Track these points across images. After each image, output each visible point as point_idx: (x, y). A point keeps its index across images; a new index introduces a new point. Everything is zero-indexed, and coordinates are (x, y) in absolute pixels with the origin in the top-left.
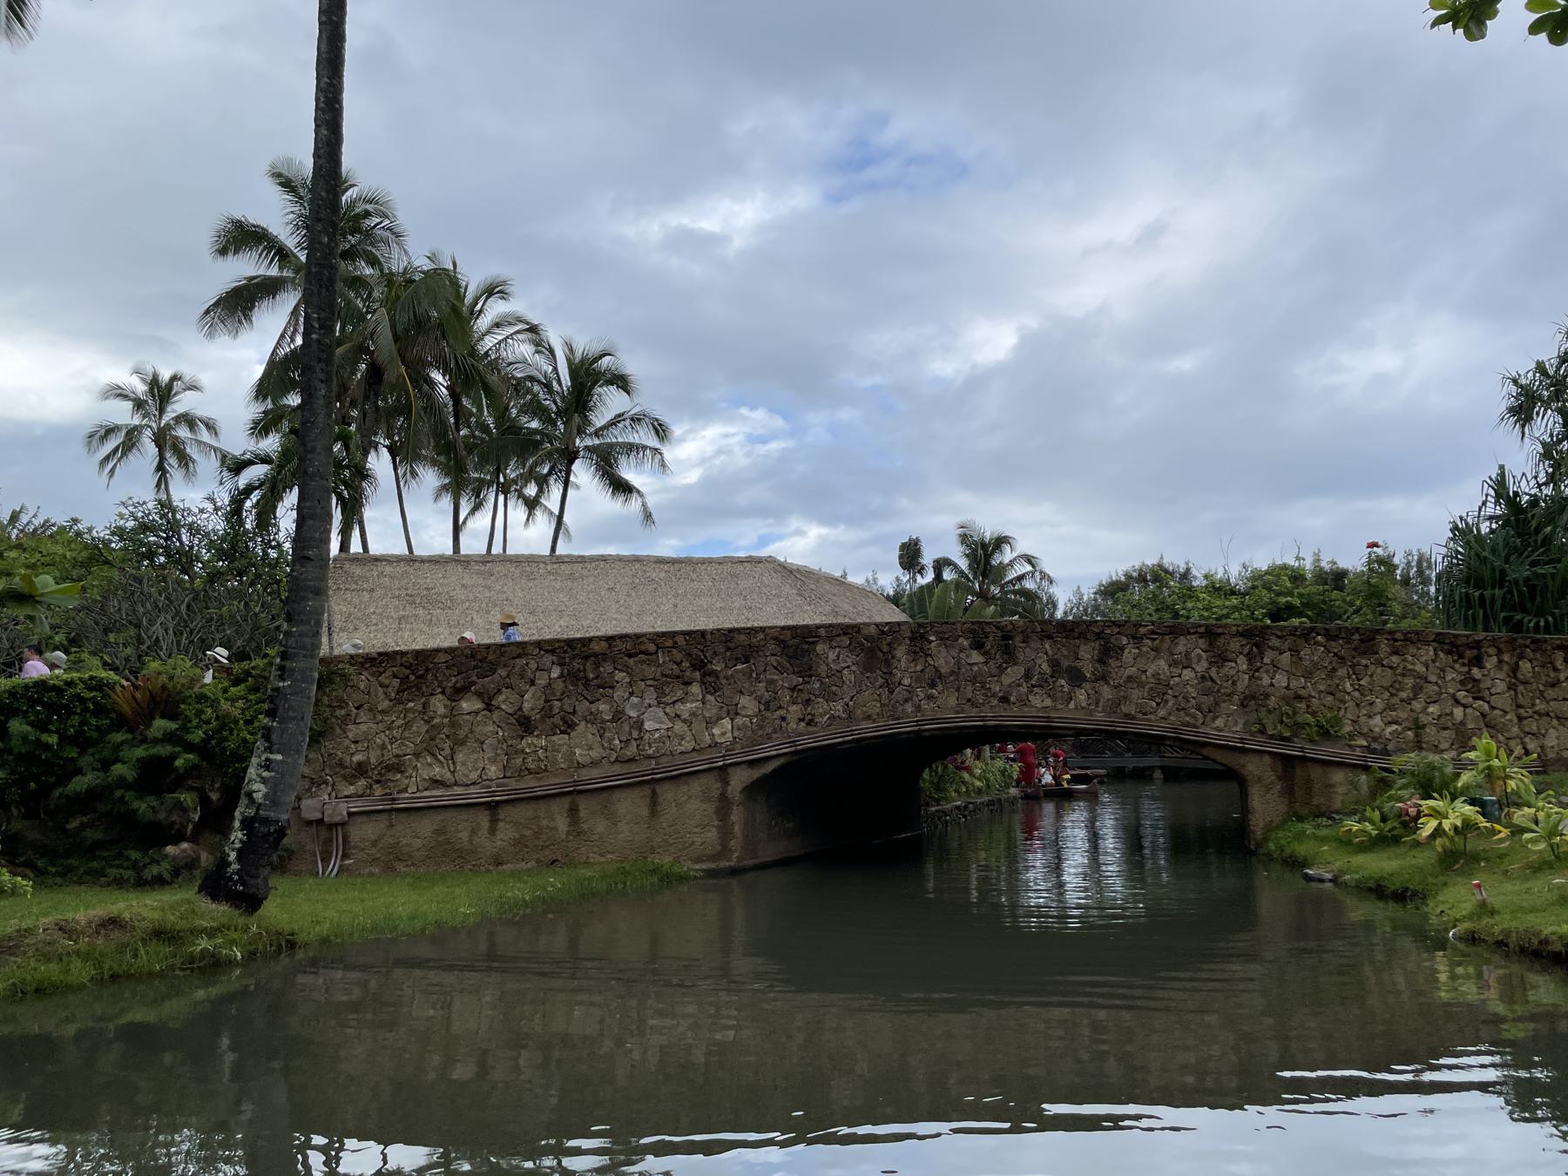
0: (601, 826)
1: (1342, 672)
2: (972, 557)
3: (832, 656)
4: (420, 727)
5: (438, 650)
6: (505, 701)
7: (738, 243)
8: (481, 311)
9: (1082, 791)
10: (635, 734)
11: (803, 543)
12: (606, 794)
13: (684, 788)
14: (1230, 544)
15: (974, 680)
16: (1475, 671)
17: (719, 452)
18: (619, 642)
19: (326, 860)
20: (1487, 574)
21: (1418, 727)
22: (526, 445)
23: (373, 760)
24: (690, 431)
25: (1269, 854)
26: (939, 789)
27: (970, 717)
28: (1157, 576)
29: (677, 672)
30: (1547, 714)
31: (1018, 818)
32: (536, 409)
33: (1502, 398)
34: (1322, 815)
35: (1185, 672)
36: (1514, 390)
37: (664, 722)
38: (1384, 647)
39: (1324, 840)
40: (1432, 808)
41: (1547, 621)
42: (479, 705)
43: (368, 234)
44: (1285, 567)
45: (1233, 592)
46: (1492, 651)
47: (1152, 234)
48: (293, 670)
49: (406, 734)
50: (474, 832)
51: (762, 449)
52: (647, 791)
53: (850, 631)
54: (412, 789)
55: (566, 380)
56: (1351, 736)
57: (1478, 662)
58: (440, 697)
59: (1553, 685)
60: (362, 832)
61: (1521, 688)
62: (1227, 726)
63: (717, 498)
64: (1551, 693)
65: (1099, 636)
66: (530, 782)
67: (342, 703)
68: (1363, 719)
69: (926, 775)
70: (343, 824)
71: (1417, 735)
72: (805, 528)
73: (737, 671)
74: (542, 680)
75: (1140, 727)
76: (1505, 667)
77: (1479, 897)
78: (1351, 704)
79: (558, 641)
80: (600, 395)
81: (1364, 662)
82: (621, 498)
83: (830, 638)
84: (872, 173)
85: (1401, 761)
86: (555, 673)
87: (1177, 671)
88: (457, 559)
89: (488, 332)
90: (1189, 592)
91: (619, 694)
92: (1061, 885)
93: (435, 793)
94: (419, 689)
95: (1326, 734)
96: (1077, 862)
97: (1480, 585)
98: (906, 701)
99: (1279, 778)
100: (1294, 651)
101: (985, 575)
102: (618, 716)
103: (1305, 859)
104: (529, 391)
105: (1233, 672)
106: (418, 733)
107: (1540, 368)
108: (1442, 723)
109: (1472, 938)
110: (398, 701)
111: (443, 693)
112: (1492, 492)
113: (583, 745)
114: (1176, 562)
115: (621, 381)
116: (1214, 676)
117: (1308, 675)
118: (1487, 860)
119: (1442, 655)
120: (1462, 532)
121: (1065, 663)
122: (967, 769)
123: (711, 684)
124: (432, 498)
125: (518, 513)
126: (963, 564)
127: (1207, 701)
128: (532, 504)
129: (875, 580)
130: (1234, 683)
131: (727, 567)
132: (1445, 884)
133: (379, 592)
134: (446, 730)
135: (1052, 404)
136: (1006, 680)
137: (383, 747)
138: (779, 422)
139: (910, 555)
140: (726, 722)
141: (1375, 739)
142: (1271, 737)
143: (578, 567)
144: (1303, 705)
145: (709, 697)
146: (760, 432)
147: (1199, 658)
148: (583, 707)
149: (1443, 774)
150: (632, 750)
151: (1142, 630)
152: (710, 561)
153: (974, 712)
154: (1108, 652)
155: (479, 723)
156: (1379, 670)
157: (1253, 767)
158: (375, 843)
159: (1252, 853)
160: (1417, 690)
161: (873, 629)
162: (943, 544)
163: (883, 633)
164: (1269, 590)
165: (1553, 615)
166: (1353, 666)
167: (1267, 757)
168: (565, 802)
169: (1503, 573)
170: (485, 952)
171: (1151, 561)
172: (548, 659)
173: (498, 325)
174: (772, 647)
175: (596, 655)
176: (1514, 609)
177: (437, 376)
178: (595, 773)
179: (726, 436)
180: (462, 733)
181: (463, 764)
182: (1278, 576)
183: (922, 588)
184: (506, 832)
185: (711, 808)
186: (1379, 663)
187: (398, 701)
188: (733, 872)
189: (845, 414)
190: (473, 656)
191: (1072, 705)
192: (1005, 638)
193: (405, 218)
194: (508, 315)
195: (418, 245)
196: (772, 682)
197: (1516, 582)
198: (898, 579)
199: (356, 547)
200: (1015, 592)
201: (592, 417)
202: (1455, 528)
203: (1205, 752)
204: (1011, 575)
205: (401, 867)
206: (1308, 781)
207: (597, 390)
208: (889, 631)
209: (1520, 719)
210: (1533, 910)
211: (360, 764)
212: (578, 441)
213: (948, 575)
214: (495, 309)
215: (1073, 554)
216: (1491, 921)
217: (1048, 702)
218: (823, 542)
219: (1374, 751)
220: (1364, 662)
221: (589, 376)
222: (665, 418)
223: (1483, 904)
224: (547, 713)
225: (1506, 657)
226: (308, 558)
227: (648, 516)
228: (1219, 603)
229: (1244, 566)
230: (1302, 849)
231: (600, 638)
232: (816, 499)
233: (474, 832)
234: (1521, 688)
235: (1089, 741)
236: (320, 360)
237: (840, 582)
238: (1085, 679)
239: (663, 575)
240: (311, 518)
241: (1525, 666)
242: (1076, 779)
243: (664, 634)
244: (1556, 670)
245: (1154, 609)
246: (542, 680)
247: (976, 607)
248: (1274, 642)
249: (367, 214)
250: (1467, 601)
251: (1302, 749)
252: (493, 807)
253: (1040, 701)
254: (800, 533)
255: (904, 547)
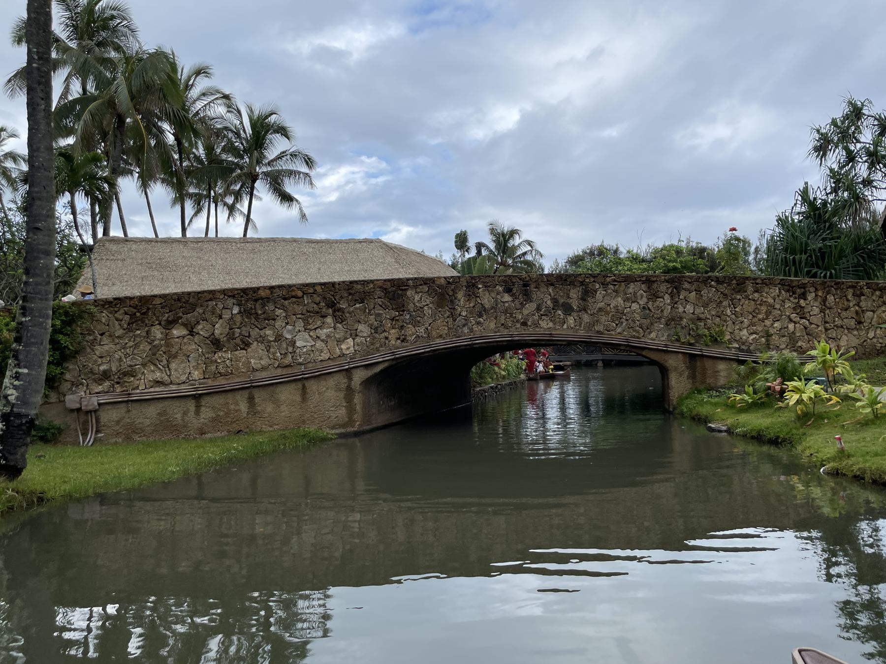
0: (270, 408)
1: (725, 303)
2: (497, 242)
3: (417, 298)
4: (145, 347)
5: (155, 296)
6: (202, 329)
7: (356, 56)
8: (192, 85)
9: (560, 375)
10: (290, 349)
11: (399, 235)
12: (271, 388)
13: (323, 383)
14: (640, 235)
15: (505, 312)
16: (802, 302)
17: (348, 182)
18: (277, 290)
19: (85, 435)
20: (798, 247)
21: (768, 335)
22: (224, 171)
23: (114, 369)
24: (331, 169)
25: (682, 414)
26: (481, 378)
27: (504, 335)
28: (602, 252)
29: (316, 308)
30: (842, 327)
31: (525, 393)
32: (230, 149)
33: (810, 140)
34: (711, 389)
35: (633, 305)
36: (817, 136)
37: (310, 342)
38: (750, 289)
39: (716, 405)
40: (795, 387)
41: (831, 273)
42: (184, 332)
43: (115, 30)
44: (672, 246)
45: (644, 260)
46: (812, 289)
47: (596, 54)
48: (32, 309)
49: (136, 352)
50: (185, 413)
51: (373, 181)
52: (300, 385)
53: (428, 282)
54: (142, 386)
55: (249, 130)
56: (730, 342)
57: (804, 296)
58: (158, 327)
59: (846, 310)
60: (109, 416)
61: (827, 311)
62: (657, 337)
63: (347, 207)
64: (844, 314)
65: (582, 283)
66: (221, 381)
67: (90, 332)
68: (737, 331)
69: (473, 370)
70: (95, 411)
71: (767, 340)
72: (400, 227)
73: (356, 309)
74: (227, 315)
75: (605, 339)
76: (819, 299)
77: (839, 446)
78: (730, 323)
79: (237, 289)
80: (270, 140)
81: (738, 297)
82: (286, 204)
83: (416, 287)
84: (435, 16)
85: (764, 356)
86: (236, 310)
87: (629, 304)
88: (184, 240)
89: (198, 99)
90: (619, 262)
91: (279, 323)
92: (545, 430)
93: (157, 389)
94: (143, 322)
95: (715, 341)
96: (556, 415)
97: (793, 252)
98: (464, 326)
99: (687, 368)
100: (698, 291)
101: (504, 253)
102: (279, 338)
103: (707, 417)
104: (225, 136)
105: (662, 304)
106: (144, 351)
107: (834, 123)
108: (781, 333)
109: (836, 474)
110: (129, 330)
111: (160, 324)
112: (800, 198)
113: (256, 357)
114: (612, 244)
115: (283, 131)
116: (650, 307)
117: (705, 305)
118: (829, 419)
119: (783, 292)
120: (782, 222)
121: (561, 301)
122: (497, 365)
123: (339, 316)
124: (169, 206)
125: (223, 214)
126: (492, 246)
127: (646, 322)
128: (232, 209)
129: (441, 256)
130: (662, 311)
131: (351, 246)
132: (805, 434)
133: (129, 261)
134: (163, 349)
135: (538, 154)
136: (525, 312)
137: (120, 360)
138: (384, 165)
139: (461, 241)
140: (350, 341)
141: (743, 344)
142: (683, 343)
143: (258, 245)
144: (702, 324)
145: (338, 325)
146: (373, 171)
147: (642, 296)
148: (255, 332)
149: (794, 364)
150: (288, 359)
151: (608, 280)
152: (341, 242)
153: (506, 332)
154: (587, 293)
155: (185, 344)
156: (747, 302)
157: (672, 362)
158: (118, 422)
159: (670, 413)
160: (768, 314)
161: (443, 281)
162: (480, 234)
163: (449, 283)
164: (664, 259)
165: (835, 269)
166: (732, 300)
167: (680, 355)
168: (246, 394)
169: (807, 244)
170: (196, 485)
171: (597, 244)
172: (230, 302)
173: (204, 94)
174: (378, 293)
175: (262, 299)
176: (812, 266)
177: (166, 126)
178: (264, 374)
179: (353, 173)
180: (174, 351)
181: (176, 370)
182: (669, 251)
183: (469, 259)
184: (206, 414)
185: (341, 395)
186: (747, 297)
187: (129, 330)
188: (356, 434)
189: (422, 160)
190: (179, 300)
191: (565, 326)
192: (525, 285)
193: (138, 19)
194: (211, 88)
195: (147, 38)
196: (379, 315)
197: (814, 250)
198: (454, 255)
199: (116, 232)
200: (521, 262)
201: (266, 153)
202: (779, 220)
203: (644, 353)
204: (519, 252)
205: (136, 438)
206: (704, 369)
207: (269, 136)
208: (451, 282)
209: (826, 330)
210: (876, 454)
211: (105, 372)
212: (257, 169)
213: (484, 253)
214: (201, 84)
215: (553, 242)
216: (850, 462)
217: (551, 325)
218: (410, 236)
219: (742, 351)
220: (738, 297)
221: (263, 129)
222: (312, 155)
223: (842, 451)
224: (231, 336)
225: (820, 293)
226: (37, 229)
227: (303, 216)
228: (636, 266)
229: (649, 246)
230: (704, 410)
231: (265, 288)
232: (408, 211)
233: (185, 413)
234: (827, 311)
235: (560, 346)
236: (39, 83)
237: (420, 255)
238: (573, 310)
239: (311, 250)
240: (40, 199)
241: (831, 298)
242: (557, 368)
243: (308, 285)
244: (848, 300)
245: (594, 274)
246: (227, 315)
247: (501, 271)
248: (686, 285)
249: (113, 17)
250: (785, 262)
251: (701, 350)
252: (197, 398)
253: (546, 324)
254: (397, 230)
255: (458, 236)
